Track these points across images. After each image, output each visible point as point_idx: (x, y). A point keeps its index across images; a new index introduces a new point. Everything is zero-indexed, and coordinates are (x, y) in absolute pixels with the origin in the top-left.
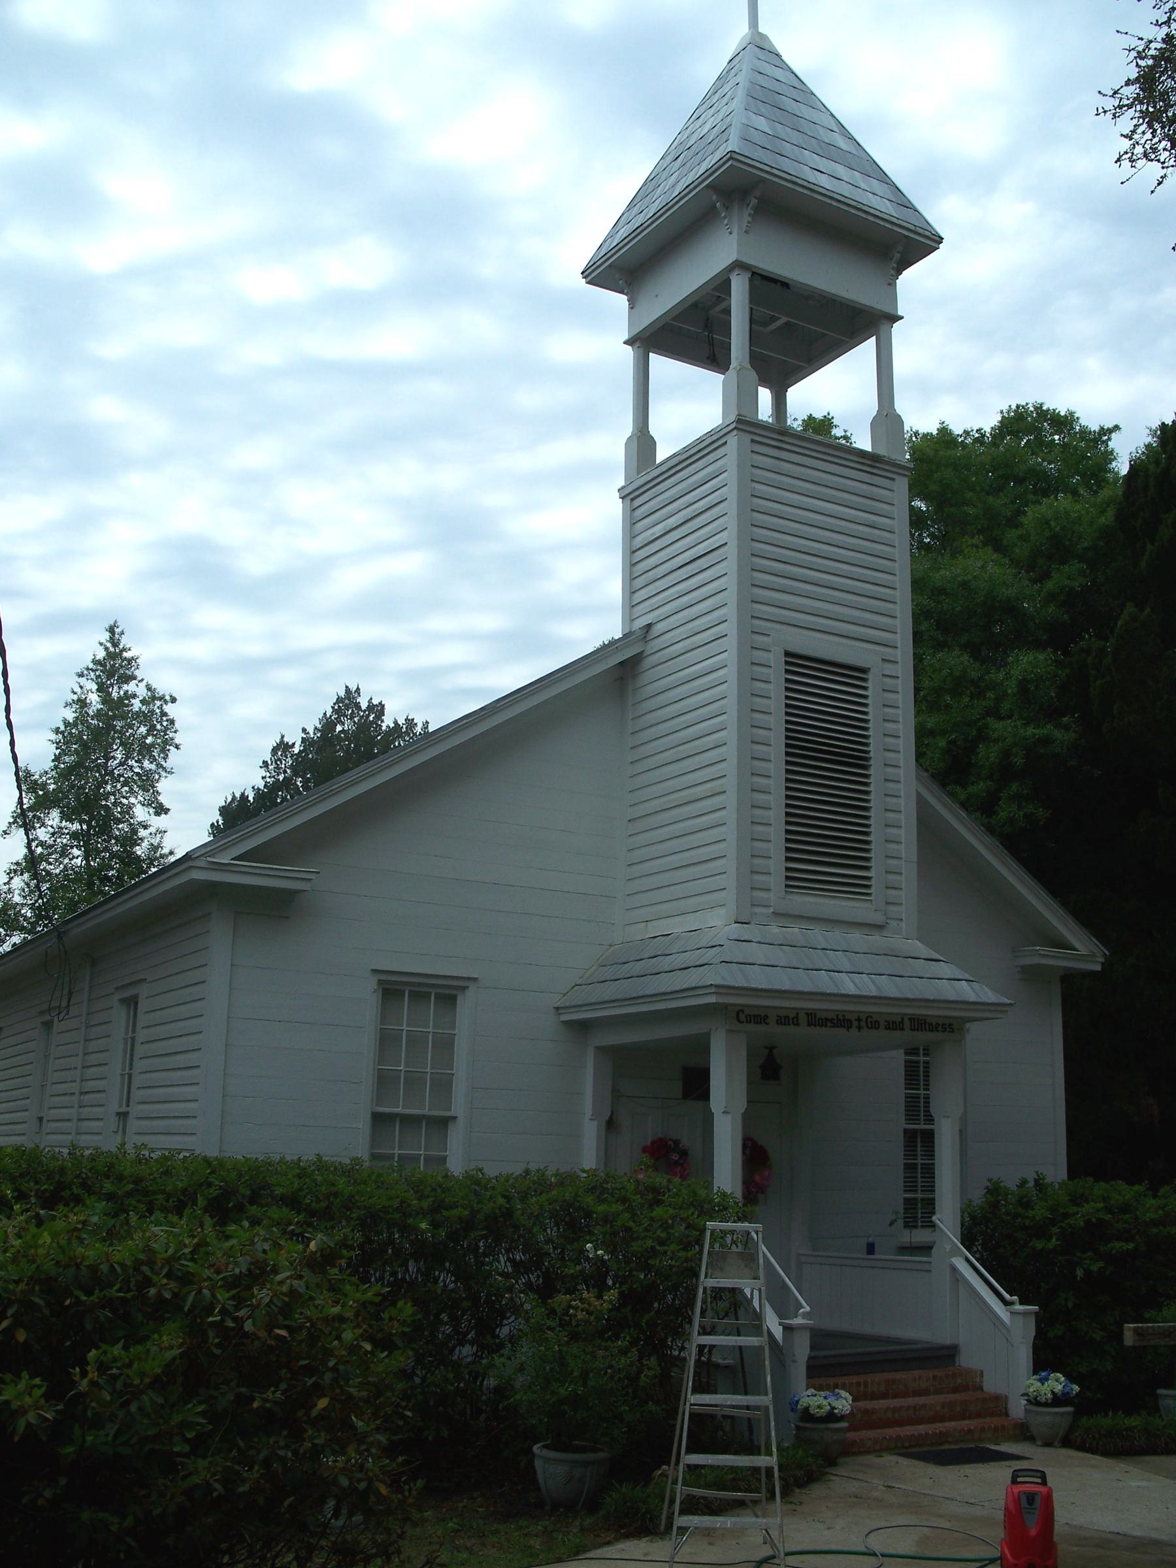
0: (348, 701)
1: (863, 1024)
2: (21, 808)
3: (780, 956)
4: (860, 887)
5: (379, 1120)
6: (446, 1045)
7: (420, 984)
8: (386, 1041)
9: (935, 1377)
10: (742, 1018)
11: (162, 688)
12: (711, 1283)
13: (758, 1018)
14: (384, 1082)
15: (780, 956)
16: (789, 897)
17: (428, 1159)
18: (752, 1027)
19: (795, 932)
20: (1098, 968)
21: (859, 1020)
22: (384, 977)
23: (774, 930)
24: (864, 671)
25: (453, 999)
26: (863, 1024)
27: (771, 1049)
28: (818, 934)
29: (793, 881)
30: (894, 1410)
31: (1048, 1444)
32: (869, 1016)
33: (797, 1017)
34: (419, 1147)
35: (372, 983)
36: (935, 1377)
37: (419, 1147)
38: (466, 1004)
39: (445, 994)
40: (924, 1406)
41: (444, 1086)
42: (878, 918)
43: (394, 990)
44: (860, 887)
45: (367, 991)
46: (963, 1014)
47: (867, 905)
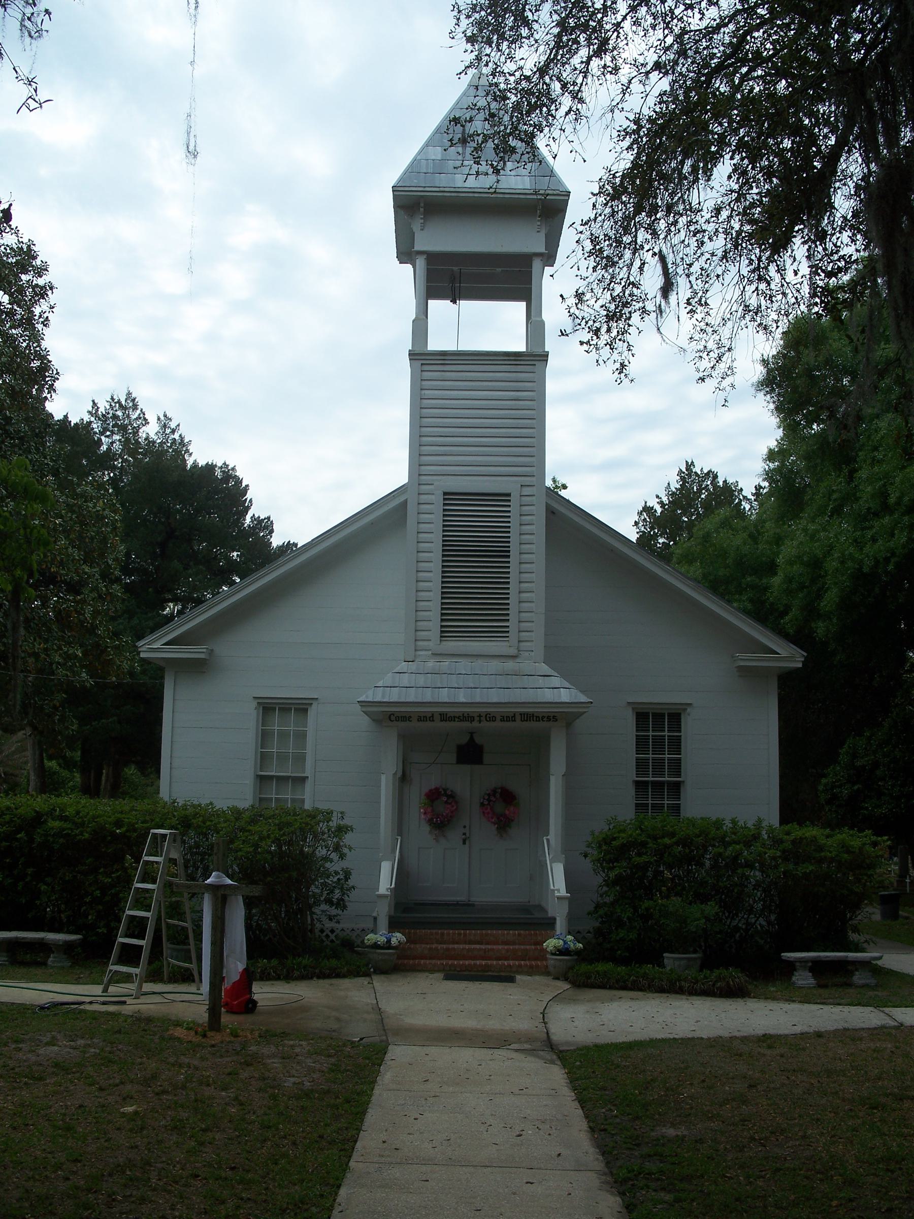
0: (688, 473)
1: (483, 718)
2: (184, 607)
3: (421, 680)
4: (503, 633)
5: (262, 780)
6: (301, 736)
7: (283, 703)
8: (264, 737)
9: (519, 935)
10: (393, 718)
11: (561, 480)
12: (146, 858)
13: (405, 718)
14: (263, 758)
15: (421, 680)
16: (444, 643)
17: (293, 800)
18: (403, 724)
19: (446, 664)
20: (800, 665)
21: (480, 716)
22: (260, 701)
23: (431, 664)
24: (509, 495)
25: (306, 710)
26: (483, 718)
27: (472, 734)
28: (463, 665)
29: (444, 633)
30: (469, 950)
31: (557, 978)
32: (487, 714)
33: (433, 716)
34: (288, 794)
35: (254, 704)
36: (519, 935)
37: (288, 794)
38: (311, 713)
39: (301, 708)
40: (492, 950)
41: (300, 759)
42: (513, 651)
43: (268, 708)
44: (503, 633)
45: (251, 711)
46: (581, 710)
47: (506, 643)
